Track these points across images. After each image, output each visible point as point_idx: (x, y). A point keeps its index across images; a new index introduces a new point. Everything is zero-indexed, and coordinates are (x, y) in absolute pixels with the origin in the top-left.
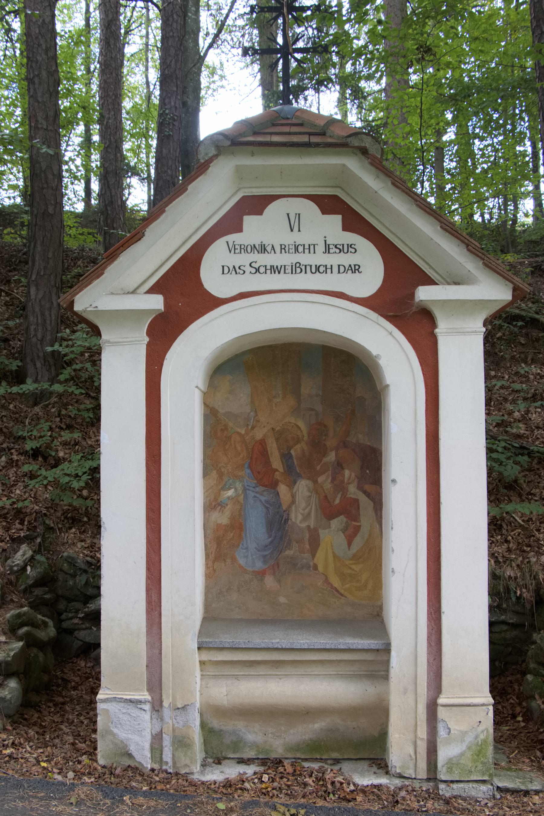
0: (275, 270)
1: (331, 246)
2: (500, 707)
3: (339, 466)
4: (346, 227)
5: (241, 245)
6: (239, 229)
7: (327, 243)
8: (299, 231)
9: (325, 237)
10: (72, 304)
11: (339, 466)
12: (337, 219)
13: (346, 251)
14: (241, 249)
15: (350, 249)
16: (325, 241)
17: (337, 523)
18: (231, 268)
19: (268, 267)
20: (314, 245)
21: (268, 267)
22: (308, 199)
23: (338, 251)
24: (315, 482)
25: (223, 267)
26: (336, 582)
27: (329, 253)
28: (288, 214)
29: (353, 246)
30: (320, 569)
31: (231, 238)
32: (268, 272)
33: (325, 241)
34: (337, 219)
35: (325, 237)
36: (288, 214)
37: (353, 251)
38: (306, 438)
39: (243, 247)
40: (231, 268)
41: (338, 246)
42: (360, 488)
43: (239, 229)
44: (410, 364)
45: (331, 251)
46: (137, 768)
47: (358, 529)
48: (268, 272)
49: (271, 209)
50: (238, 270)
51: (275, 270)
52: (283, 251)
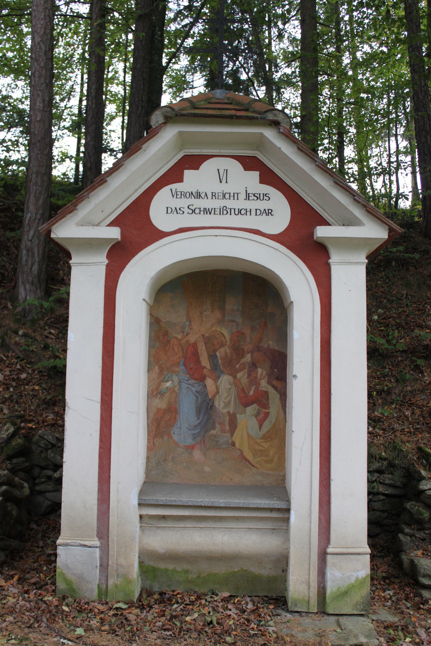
0: (207, 211)
1: (250, 195)
3: (254, 365)
4: (263, 181)
6: (181, 180)
7: (248, 192)
10: (49, 232)
11: (254, 365)
12: (256, 175)
13: (262, 198)
14: (181, 195)
15: (265, 197)
16: (246, 191)
17: (251, 410)
23: (256, 198)
24: (235, 377)
25: (167, 208)
26: (249, 455)
27: (249, 199)
28: (218, 170)
29: (267, 195)
30: (237, 445)
31: (174, 186)
33: (246, 191)
34: (256, 175)
36: (218, 170)
37: (267, 198)
38: (228, 343)
39: (183, 193)
41: (256, 195)
42: (269, 383)
43: (181, 180)
45: (250, 198)
47: (267, 415)
49: (206, 166)
51: (207, 211)
52: (214, 197)
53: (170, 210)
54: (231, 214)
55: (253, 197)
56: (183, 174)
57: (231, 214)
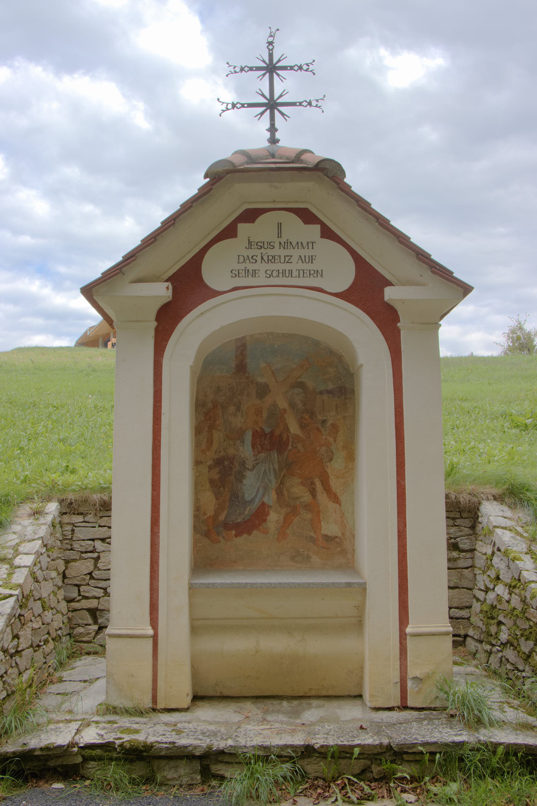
1: (253, 243)
2: (155, 493)
5: (310, 270)
7: (250, 241)
8: (313, 248)
9: (249, 237)
16: (249, 240)
18: (246, 257)
19: (281, 271)
21: (281, 271)
22: (297, 214)
27: (251, 248)
32: (281, 275)
33: (249, 240)
37: (259, 244)
40: (246, 257)
44: (214, 307)
45: (253, 247)
46: (353, 719)
48: (281, 275)
50: (251, 260)
53: (241, 259)
55: (256, 247)
56: (318, 224)
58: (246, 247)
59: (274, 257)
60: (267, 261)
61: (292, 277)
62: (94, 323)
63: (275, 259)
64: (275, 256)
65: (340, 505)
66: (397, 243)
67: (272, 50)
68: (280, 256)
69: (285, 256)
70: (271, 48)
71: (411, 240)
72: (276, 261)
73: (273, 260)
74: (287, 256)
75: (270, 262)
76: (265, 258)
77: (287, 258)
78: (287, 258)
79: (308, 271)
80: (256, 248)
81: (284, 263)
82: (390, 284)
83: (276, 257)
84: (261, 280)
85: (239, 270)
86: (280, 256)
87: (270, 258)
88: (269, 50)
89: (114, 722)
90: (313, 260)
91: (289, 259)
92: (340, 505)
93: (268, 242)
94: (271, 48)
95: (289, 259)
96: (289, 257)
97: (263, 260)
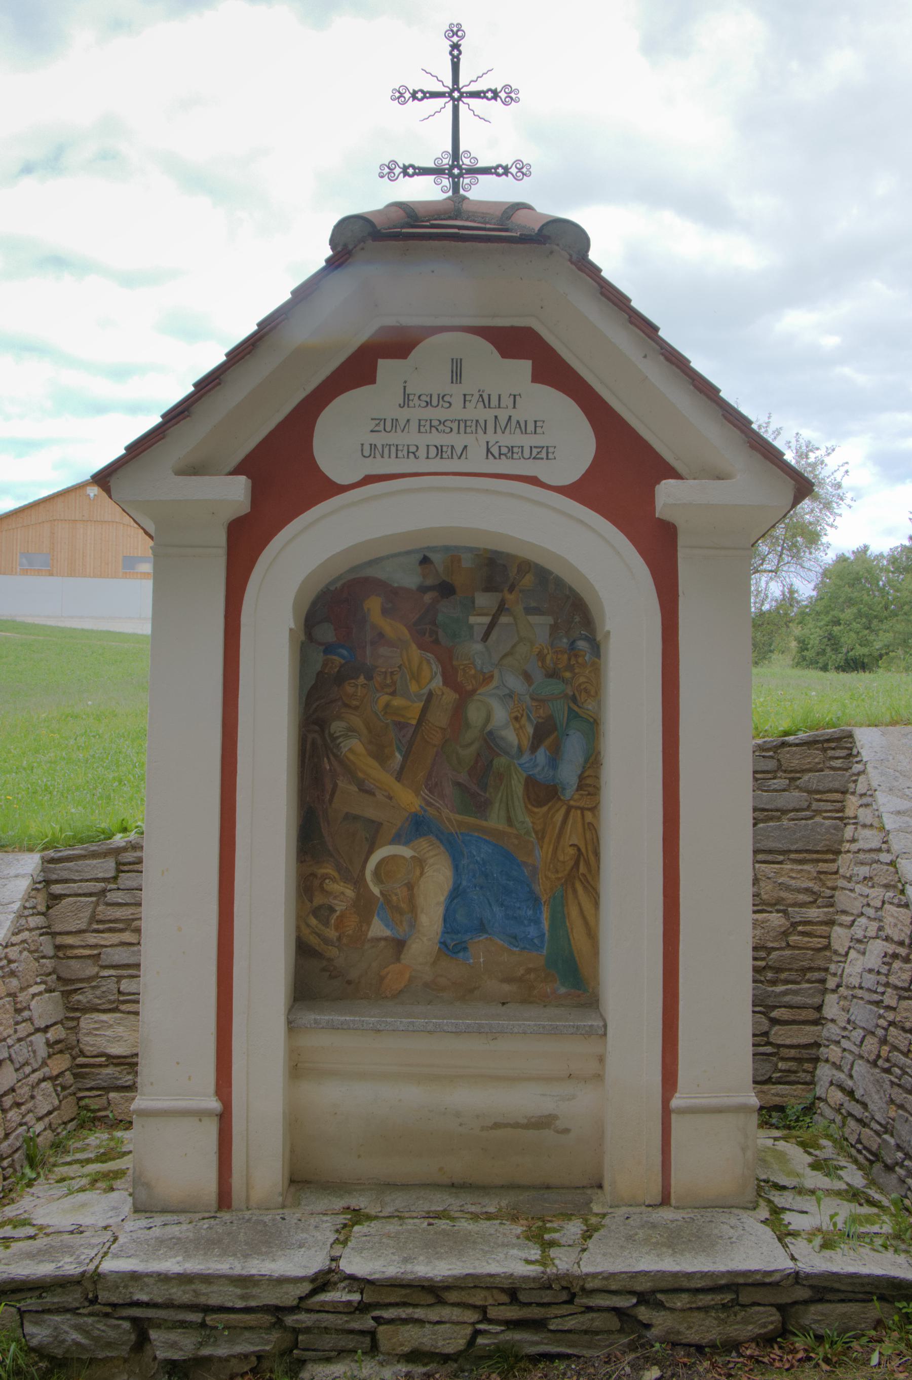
1: (411, 397)
6: (370, 379)
7: (407, 393)
9: (405, 382)
12: (525, 366)
14: (431, 426)
16: (405, 387)
20: (515, 396)
33: (405, 387)
34: (525, 366)
35: (405, 382)
45: (411, 404)
53: (433, 451)
54: (459, 432)
57: (459, 432)
58: (400, 405)
59: (511, 449)
60: (497, 456)
61: (442, 458)
62: (128, 628)
63: (513, 453)
64: (512, 447)
65: (762, 1222)
66: (691, 387)
67: (458, 57)
68: (522, 447)
69: (531, 447)
70: (487, 95)
71: (785, 457)
72: (515, 456)
73: (510, 454)
74: (535, 447)
75: (411, 455)
76: (495, 451)
77: (535, 451)
78: (535, 451)
79: (429, 422)
80: (417, 405)
81: (529, 458)
82: (672, 473)
83: (515, 450)
84: (477, 461)
85: (408, 446)
86: (522, 447)
87: (504, 450)
88: (453, 57)
89: (811, 934)
90: (467, 403)
91: (538, 453)
92: (762, 1222)
93: (439, 395)
94: (487, 95)
95: (538, 453)
96: (539, 450)
97: (489, 454)
